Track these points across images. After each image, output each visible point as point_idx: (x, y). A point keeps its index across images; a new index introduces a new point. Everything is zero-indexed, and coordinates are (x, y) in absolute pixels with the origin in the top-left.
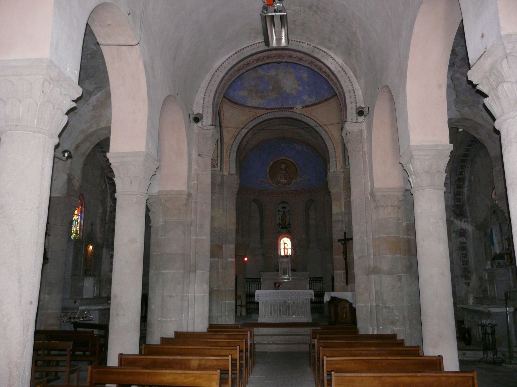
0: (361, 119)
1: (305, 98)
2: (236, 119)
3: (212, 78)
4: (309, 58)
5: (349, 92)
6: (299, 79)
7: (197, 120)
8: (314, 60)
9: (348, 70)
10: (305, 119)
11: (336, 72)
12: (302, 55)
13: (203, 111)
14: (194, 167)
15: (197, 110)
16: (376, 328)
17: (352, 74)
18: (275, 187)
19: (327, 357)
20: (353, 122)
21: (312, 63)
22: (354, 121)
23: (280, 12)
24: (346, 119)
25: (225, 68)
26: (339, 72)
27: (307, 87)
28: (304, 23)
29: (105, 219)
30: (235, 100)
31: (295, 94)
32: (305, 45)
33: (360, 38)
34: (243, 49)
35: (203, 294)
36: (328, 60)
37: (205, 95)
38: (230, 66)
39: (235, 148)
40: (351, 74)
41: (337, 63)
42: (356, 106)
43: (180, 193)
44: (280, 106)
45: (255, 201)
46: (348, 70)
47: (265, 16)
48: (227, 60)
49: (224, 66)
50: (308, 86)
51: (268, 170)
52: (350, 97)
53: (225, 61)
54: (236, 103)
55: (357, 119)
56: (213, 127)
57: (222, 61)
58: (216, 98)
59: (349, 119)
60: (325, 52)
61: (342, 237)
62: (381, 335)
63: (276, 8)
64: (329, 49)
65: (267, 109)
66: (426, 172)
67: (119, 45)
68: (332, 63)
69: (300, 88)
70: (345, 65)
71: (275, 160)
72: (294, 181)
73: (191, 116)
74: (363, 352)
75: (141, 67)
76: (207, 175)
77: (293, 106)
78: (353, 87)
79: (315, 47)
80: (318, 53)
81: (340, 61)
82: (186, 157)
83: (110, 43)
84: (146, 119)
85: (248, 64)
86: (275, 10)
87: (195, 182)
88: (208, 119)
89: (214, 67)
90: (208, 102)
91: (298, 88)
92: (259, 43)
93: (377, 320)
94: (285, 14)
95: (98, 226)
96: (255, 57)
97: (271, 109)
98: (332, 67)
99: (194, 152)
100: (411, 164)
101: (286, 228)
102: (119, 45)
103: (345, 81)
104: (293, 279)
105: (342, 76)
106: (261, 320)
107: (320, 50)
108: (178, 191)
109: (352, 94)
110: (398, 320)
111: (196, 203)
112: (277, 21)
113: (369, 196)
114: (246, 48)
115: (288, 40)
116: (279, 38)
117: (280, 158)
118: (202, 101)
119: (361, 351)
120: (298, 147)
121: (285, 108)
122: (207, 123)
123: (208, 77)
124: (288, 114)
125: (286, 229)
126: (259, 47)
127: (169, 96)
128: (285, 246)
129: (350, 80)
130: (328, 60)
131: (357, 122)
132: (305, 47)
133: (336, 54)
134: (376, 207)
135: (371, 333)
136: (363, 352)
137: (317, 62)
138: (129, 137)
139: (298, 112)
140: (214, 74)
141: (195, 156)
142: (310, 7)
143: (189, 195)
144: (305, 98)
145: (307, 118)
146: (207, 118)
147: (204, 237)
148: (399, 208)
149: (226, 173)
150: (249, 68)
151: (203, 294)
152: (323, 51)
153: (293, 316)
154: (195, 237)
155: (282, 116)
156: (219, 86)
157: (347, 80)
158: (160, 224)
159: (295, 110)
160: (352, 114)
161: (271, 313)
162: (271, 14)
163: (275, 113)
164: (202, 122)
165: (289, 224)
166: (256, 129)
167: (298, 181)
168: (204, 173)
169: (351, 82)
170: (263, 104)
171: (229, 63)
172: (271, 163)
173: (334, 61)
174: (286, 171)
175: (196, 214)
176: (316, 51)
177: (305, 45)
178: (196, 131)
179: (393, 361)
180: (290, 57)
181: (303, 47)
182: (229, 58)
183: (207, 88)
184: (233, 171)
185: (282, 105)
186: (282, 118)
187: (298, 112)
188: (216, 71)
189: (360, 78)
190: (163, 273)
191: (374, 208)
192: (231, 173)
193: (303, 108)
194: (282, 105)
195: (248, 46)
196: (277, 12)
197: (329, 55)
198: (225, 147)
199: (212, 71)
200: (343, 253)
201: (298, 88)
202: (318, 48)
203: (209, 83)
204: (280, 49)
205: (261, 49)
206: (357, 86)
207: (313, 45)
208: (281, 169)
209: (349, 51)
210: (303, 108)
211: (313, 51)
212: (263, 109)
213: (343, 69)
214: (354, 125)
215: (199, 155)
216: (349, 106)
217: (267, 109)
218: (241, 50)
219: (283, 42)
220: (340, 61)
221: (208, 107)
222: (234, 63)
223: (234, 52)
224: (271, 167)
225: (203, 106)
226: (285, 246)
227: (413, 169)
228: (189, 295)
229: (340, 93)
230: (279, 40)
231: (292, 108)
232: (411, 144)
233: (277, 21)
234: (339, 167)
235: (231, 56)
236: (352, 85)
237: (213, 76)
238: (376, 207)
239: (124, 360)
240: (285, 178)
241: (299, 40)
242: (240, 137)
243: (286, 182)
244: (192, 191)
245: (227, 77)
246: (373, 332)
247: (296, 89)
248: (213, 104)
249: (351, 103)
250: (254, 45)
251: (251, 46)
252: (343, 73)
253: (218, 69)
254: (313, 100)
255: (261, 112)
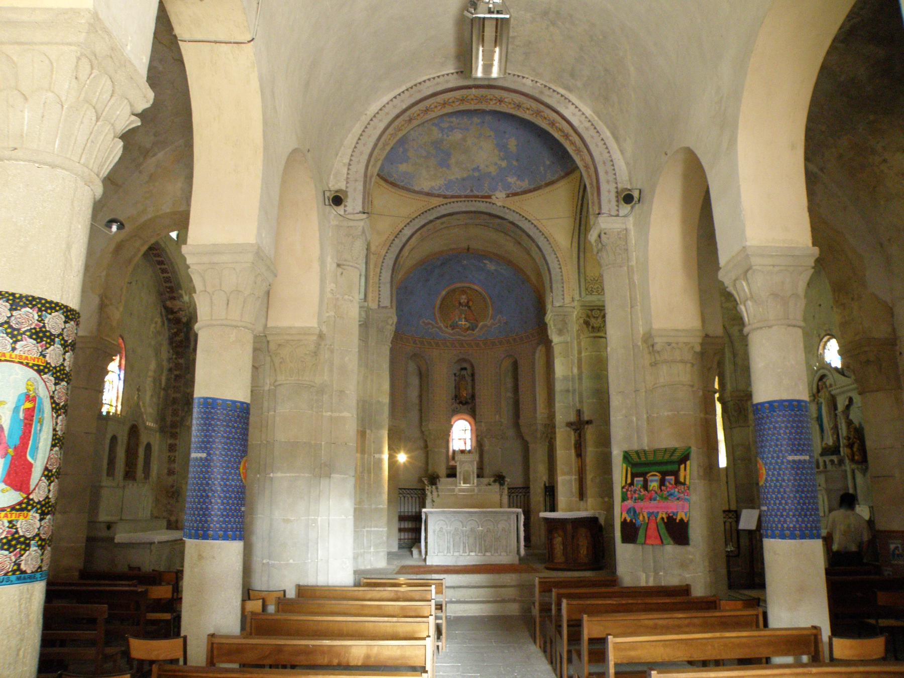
0: (625, 209)
1: (511, 180)
2: (398, 210)
3: (364, 131)
4: (535, 105)
5: (604, 163)
6: (502, 147)
7: (337, 200)
8: (542, 107)
9: (601, 126)
10: (510, 217)
11: (581, 130)
12: (522, 99)
13: (347, 187)
14: (330, 286)
15: (336, 184)
16: (652, 574)
17: (608, 134)
18: (450, 334)
19: (615, 636)
20: (612, 216)
21: (538, 113)
22: (614, 213)
23: (498, 12)
24: (600, 208)
25: (387, 114)
26: (587, 129)
27: (515, 163)
28: (530, 42)
29: (161, 381)
30: (392, 180)
31: (494, 173)
32: (528, 82)
33: (632, 69)
34: (420, 83)
35: (343, 517)
36: (567, 108)
37: (351, 160)
38: (397, 111)
39: (390, 262)
40: (607, 133)
41: (583, 114)
42: (617, 188)
43: (305, 332)
44: (468, 192)
45: (415, 356)
46: (601, 126)
47: (472, 20)
48: (391, 100)
49: (386, 110)
50: (517, 160)
51: (439, 302)
52: (607, 173)
53: (388, 103)
54: (393, 184)
55: (618, 210)
56: (365, 216)
57: (383, 102)
58: (370, 167)
59: (605, 209)
60: (562, 96)
61: (572, 418)
62: (662, 587)
63: (491, 6)
64: (570, 90)
65: (445, 197)
66: (775, 295)
67: (216, 42)
68: (574, 114)
69: (504, 164)
70: (596, 118)
71: (452, 287)
72: (481, 324)
73: (327, 194)
74: (661, 622)
75: (255, 84)
76: (352, 301)
77: (491, 193)
78: (610, 156)
79: (545, 86)
80: (550, 96)
81: (588, 112)
82: (316, 266)
83: (199, 38)
84: (258, 183)
85: (427, 110)
86: (490, 9)
87: (332, 313)
88: (354, 203)
89: (368, 113)
90: (356, 172)
91: (499, 162)
92: (448, 75)
93: (655, 562)
94: (508, 16)
95: (149, 394)
96: (439, 99)
97: (452, 197)
98: (575, 121)
99: (329, 259)
100: (747, 280)
101: (467, 403)
102: (216, 42)
103: (597, 145)
104: (480, 491)
105: (592, 137)
106: (433, 560)
107: (554, 91)
108: (302, 328)
109: (610, 169)
110: (692, 561)
111: (332, 352)
112: (489, 31)
113: (640, 344)
114: (424, 81)
115: (504, 68)
116: (489, 65)
117: (458, 285)
118: (345, 171)
119: (656, 621)
120: (491, 267)
121: (477, 197)
122: (354, 209)
123: (357, 129)
124: (482, 206)
125: (465, 404)
126: (447, 82)
127: (295, 151)
128: (461, 434)
129: (605, 144)
130: (567, 108)
131: (617, 216)
132: (527, 85)
133: (580, 98)
134: (654, 364)
135: (643, 584)
136: (661, 622)
137: (548, 112)
138: (227, 216)
139: (499, 204)
140: (369, 124)
141: (330, 265)
142: (545, 13)
143: (321, 336)
144: (511, 180)
145: (515, 214)
146: (354, 199)
147: (346, 414)
148: (693, 365)
149: (374, 306)
150: (428, 117)
151: (343, 517)
152: (558, 93)
153: (488, 554)
154: (329, 413)
155: (473, 209)
156: (376, 145)
157: (601, 144)
158: (267, 388)
159: (494, 199)
160: (610, 201)
161: (448, 548)
162: (482, 16)
163: (459, 204)
164: (345, 206)
165: (473, 396)
166: (428, 226)
167: (489, 324)
168: (346, 297)
169: (607, 148)
170: (440, 188)
171: (394, 107)
172: (444, 293)
173: (578, 110)
174: (469, 307)
175: (331, 371)
176: (547, 92)
177: (528, 82)
178: (334, 223)
179: (733, 640)
180: (501, 101)
181: (524, 84)
182: (395, 97)
183: (355, 147)
184: (386, 302)
185: (472, 191)
186: (471, 212)
187: (499, 204)
188: (371, 120)
189: (625, 140)
190: (272, 479)
191: (651, 365)
192: (382, 305)
193: (508, 196)
194: (472, 191)
195: (429, 80)
196: (493, 13)
197: (570, 101)
198: (373, 258)
199: (365, 119)
200: (575, 444)
201: (499, 162)
202: (550, 88)
203: (359, 139)
204: (489, 85)
205: (451, 85)
206: (617, 155)
207: (541, 82)
208: (460, 304)
209: (605, 91)
210: (508, 196)
211: (541, 92)
212: (439, 196)
213: (592, 125)
214: (610, 221)
215: (338, 265)
216: (604, 187)
217: (445, 197)
218: (416, 85)
219: (495, 73)
220: (588, 112)
221: (356, 180)
222: (404, 107)
223: (404, 88)
224: (444, 299)
225: (347, 178)
226: (461, 434)
227: (750, 289)
228: (319, 519)
229: (587, 167)
230: (488, 67)
231: (489, 197)
232: (748, 244)
233: (489, 31)
234: (568, 299)
235: (399, 95)
236: (609, 152)
237: (366, 127)
238: (654, 364)
239: (218, 649)
240: (466, 320)
241: (517, 73)
242: (399, 243)
243: (468, 325)
244: (324, 329)
245: (390, 130)
246: (647, 582)
247: (496, 164)
248: (366, 176)
249: (608, 182)
250: (438, 77)
251: (434, 78)
252: (592, 132)
253: (375, 116)
254: (525, 184)
255: (435, 201)
